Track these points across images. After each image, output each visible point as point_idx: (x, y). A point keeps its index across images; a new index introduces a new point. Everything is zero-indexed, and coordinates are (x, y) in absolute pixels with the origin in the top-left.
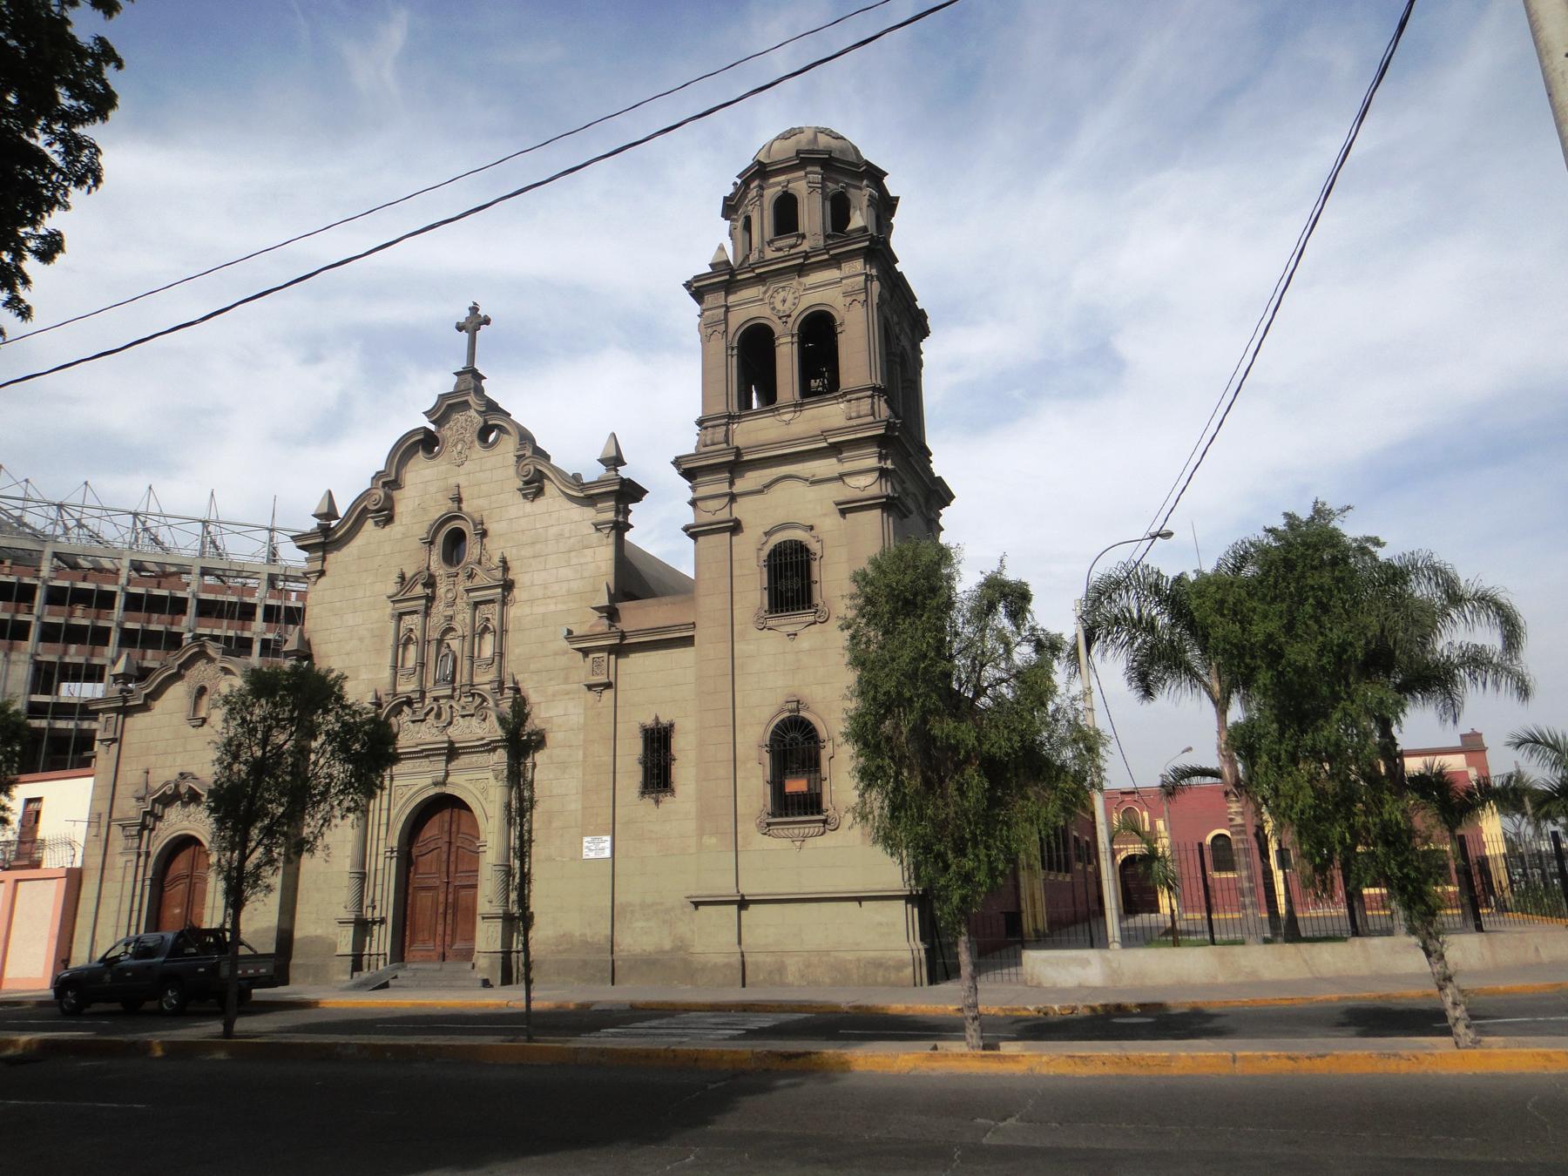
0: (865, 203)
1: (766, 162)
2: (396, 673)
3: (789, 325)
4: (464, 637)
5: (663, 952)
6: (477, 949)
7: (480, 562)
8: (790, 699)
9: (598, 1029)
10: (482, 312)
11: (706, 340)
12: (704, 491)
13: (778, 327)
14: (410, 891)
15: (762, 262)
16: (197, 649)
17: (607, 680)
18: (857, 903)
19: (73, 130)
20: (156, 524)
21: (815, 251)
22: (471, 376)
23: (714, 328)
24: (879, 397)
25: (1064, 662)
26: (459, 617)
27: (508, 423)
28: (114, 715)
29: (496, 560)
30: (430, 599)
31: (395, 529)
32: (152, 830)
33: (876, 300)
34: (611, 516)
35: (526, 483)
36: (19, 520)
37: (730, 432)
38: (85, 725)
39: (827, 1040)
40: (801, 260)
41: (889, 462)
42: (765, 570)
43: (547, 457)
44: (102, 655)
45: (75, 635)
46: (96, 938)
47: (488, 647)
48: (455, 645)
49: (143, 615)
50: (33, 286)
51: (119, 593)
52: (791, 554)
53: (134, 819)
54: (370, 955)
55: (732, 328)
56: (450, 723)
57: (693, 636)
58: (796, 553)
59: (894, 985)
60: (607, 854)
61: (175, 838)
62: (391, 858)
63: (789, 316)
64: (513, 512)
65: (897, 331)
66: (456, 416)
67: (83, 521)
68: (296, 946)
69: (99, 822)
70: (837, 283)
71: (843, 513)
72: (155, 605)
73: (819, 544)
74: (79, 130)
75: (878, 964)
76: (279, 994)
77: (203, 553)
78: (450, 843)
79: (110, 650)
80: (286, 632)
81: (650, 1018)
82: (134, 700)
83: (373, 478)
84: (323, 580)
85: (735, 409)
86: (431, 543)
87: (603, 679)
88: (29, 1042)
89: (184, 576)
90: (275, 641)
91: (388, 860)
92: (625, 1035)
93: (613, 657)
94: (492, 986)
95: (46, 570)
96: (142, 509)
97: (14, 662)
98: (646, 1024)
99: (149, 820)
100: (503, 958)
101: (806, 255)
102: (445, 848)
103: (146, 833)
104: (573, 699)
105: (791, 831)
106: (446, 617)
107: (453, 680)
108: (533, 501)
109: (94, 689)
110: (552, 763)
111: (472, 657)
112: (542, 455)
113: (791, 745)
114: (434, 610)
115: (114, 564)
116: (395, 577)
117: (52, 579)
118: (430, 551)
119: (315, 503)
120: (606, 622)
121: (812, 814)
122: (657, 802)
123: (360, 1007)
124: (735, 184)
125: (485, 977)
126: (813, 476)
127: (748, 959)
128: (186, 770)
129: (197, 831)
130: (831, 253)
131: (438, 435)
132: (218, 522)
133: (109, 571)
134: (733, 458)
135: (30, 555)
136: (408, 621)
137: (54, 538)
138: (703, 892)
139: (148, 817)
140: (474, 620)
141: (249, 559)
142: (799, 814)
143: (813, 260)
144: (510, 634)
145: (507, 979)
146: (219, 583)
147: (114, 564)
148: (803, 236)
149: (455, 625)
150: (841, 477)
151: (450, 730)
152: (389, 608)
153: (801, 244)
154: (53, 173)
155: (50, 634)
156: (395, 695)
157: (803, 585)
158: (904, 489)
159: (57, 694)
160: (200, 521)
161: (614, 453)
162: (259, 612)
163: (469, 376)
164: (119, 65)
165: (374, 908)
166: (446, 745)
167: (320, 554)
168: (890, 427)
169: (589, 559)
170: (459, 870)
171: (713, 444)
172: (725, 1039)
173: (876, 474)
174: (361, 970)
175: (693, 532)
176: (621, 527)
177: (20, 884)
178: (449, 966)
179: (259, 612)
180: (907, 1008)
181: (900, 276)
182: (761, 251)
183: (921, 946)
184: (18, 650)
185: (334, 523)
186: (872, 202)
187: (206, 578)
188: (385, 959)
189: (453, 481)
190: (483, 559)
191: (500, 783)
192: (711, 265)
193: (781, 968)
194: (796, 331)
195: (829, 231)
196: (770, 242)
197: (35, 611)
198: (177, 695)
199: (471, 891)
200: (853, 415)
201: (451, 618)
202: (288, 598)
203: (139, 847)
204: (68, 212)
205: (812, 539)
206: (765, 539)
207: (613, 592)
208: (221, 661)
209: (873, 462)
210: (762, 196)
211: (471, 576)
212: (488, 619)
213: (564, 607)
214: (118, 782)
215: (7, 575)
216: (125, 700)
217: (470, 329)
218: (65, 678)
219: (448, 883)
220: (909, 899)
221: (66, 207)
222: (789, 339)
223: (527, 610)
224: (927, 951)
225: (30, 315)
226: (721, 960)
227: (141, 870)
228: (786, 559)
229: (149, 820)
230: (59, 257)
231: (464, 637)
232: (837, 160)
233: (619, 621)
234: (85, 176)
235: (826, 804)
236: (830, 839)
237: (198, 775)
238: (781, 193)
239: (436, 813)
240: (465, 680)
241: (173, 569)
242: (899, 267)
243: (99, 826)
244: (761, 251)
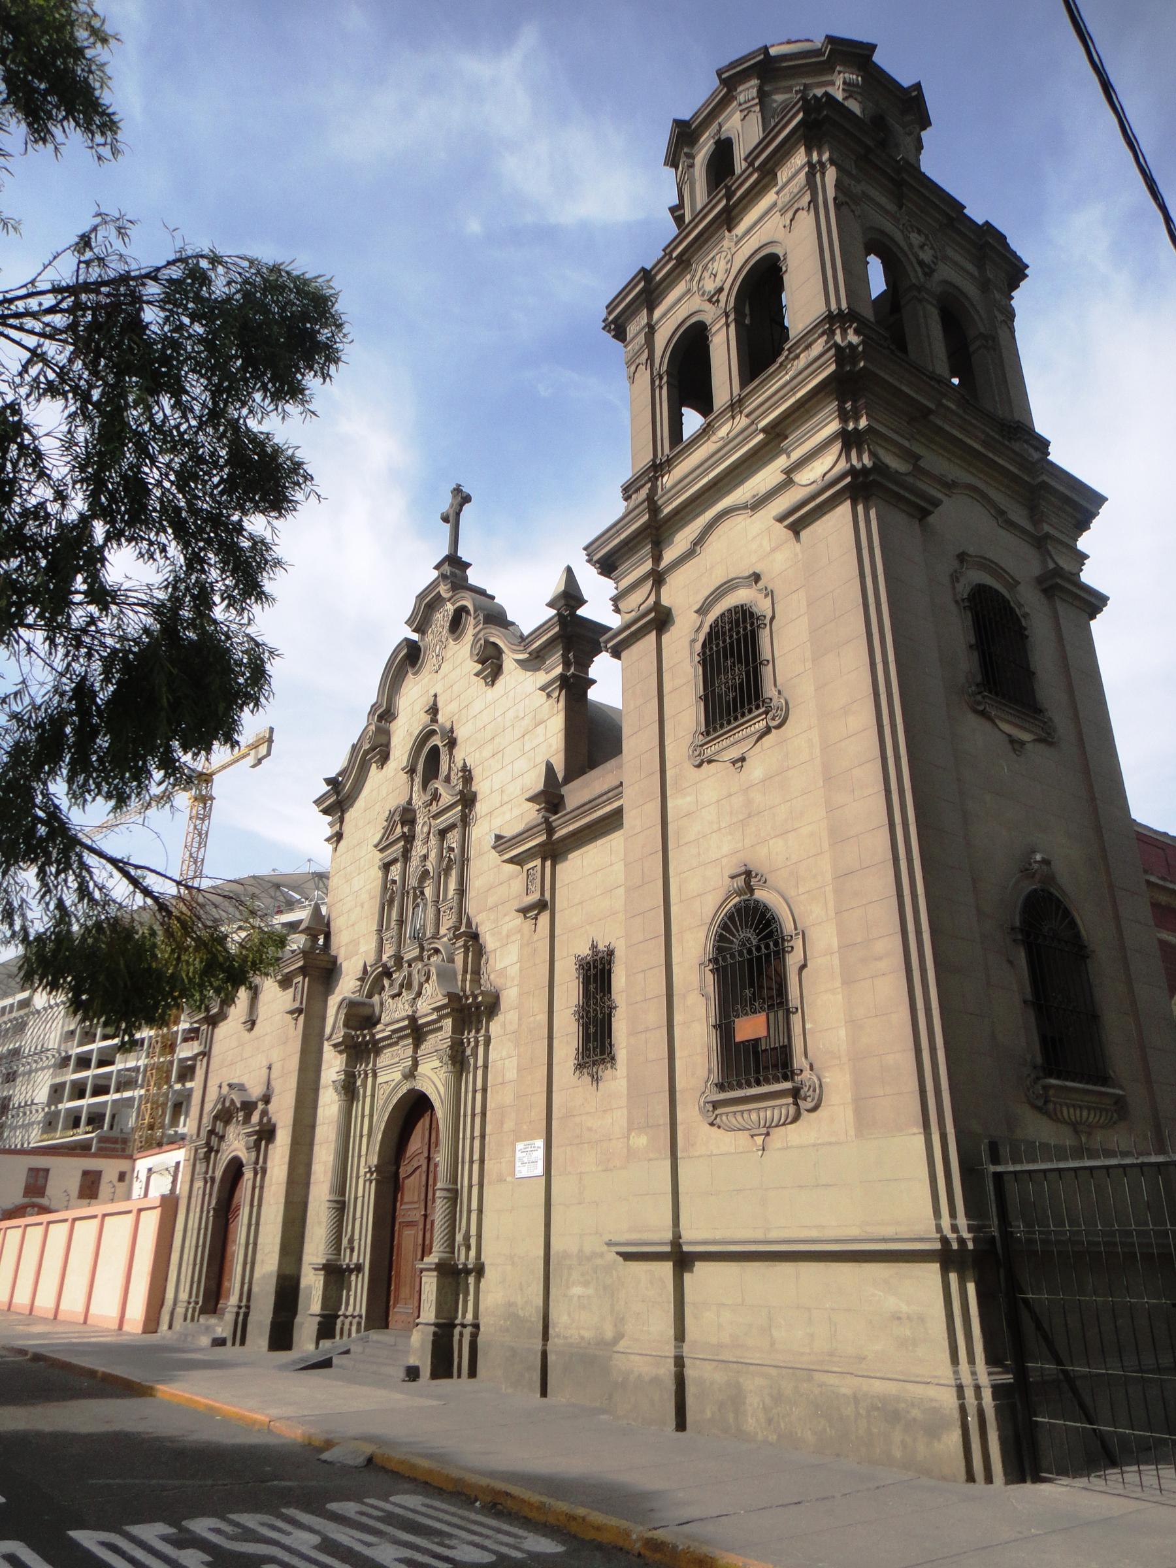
25: (843, 465)
32: (217, 1152)
52: (731, 630)
54: (346, 1317)
58: (738, 625)
64: (478, 706)
99: (214, 1141)
100: (435, 1334)
110: (505, 1035)
144: (472, 863)
166: (406, 1023)
173: (837, 447)
174: (333, 1337)
235: (799, 1061)
238: (714, 147)
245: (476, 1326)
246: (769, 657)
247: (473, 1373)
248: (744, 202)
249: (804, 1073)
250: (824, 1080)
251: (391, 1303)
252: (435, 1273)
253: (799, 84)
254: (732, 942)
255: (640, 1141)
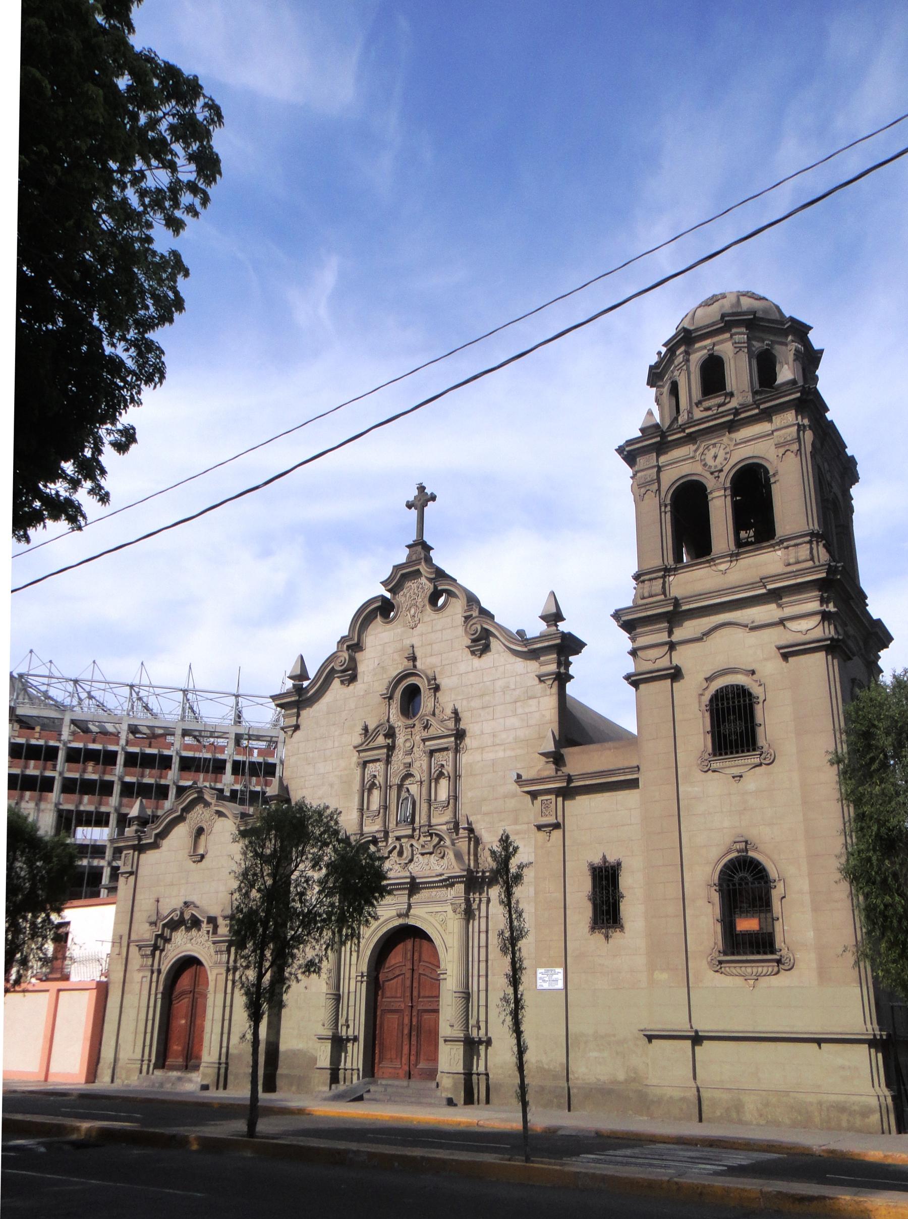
0: (791, 357)
1: (692, 328)
2: (362, 815)
3: (722, 479)
4: (421, 782)
5: (615, 1082)
6: (440, 1069)
7: (434, 714)
8: (737, 840)
9: (578, 1154)
10: (428, 491)
11: (639, 499)
12: (642, 641)
13: (710, 483)
14: (379, 1013)
15: (691, 422)
16: (196, 795)
17: (555, 821)
18: (815, 1045)
19: (146, 336)
20: (146, 694)
21: (745, 407)
22: (421, 548)
23: (648, 488)
24: (817, 542)
26: (417, 764)
27: (456, 587)
28: (131, 852)
29: (449, 712)
30: (391, 748)
31: (358, 687)
33: (809, 448)
34: (553, 667)
35: (473, 641)
36: (46, 694)
37: (667, 585)
38: (95, 863)
39: (818, 1183)
40: (731, 417)
41: (831, 605)
42: (707, 715)
43: (492, 617)
44: (107, 804)
45: (87, 787)
46: (120, 1042)
47: (443, 791)
48: (414, 789)
49: (138, 770)
50: (108, 476)
51: (119, 752)
52: (733, 698)
53: (147, 941)
55: (665, 486)
56: (411, 861)
57: (638, 779)
59: (859, 1131)
60: (560, 985)
61: (185, 956)
62: (362, 982)
63: (721, 471)
64: (463, 667)
65: (829, 479)
66: (408, 584)
67: (92, 693)
68: (282, 1057)
69: (120, 943)
70: (768, 435)
71: (785, 657)
72: (147, 761)
73: (761, 689)
74: (150, 335)
75: (842, 1108)
76: (271, 1100)
77: (184, 717)
78: (413, 970)
79: (114, 800)
80: (250, 782)
81: (628, 1146)
82: (146, 839)
83: (339, 643)
84: (298, 733)
85: (670, 562)
86: (390, 698)
87: (551, 820)
88: (89, 1130)
89: (168, 737)
90: (241, 791)
91: (359, 984)
92: (605, 1162)
93: (560, 799)
94: (456, 1105)
95: (65, 735)
96: (136, 682)
97: (43, 811)
98: (618, 1152)
99: (160, 942)
101: (736, 412)
102: (408, 975)
103: (157, 953)
104: (523, 838)
105: (743, 969)
106: (405, 764)
107: (413, 821)
108: (480, 657)
109: (101, 833)
111: (429, 801)
112: (485, 614)
113: (740, 884)
114: (394, 759)
115: (115, 728)
116: (359, 729)
117: (70, 741)
118: (389, 706)
119: (290, 666)
120: (553, 767)
121: (765, 953)
122: (607, 937)
123: (345, 1115)
124: (659, 353)
125: (450, 1096)
126: (753, 622)
127: (705, 1094)
128: (187, 899)
129: (199, 953)
130: (762, 407)
131: (394, 602)
132: (195, 691)
133: (111, 734)
134: (671, 608)
135: (54, 722)
136: (372, 768)
137: (72, 708)
138: (656, 1026)
139: (159, 939)
140: (431, 765)
141: (219, 721)
142: (753, 954)
143: (743, 416)
144: (462, 779)
145: (469, 1099)
146: (196, 743)
147: (115, 728)
148: (731, 395)
149: (413, 771)
150: (782, 622)
151: (411, 867)
152: (355, 758)
153: (729, 402)
154: (128, 376)
155: (69, 786)
156: (362, 834)
157: (746, 728)
158: (846, 633)
159: (74, 837)
160: (181, 690)
161: (554, 610)
162: (229, 767)
163: (419, 548)
164: (187, 274)
165: (348, 1027)
166: (408, 880)
167: (295, 710)
168: (831, 570)
169: (534, 709)
170: (422, 995)
171: (651, 596)
172: (711, 1174)
173: (818, 618)
175: (635, 681)
176: (562, 678)
177: (61, 993)
178: (415, 1084)
179: (229, 767)
180: (885, 1156)
181: (831, 424)
182: (690, 412)
183: (887, 1093)
184: (46, 800)
185: (306, 684)
186: (798, 355)
187: (186, 738)
188: (358, 1074)
189: (407, 643)
190: (437, 711)
191: (459, 916)
192: (642, 430)
193: (739, 1107)
194: (728, 485)
195: (757, 386)
196: (698, 404)
197: (58, 768)
198: (181, 834)
199: (432, 1016)
200: (792, 561)
201: (410, 765)
202: (251, 754)
203: (152, 965)
204: (141, 408)
205: (754, 683)
206: (705, 685)
207: (557, 738)
208: (216, 805)
209: (815, 606)
210: (688, 361)
211: (426, 727)
212: (442, 766)
213: (512, 754)
214: (135, 909)
215: (37, 739)
216: (140, 839)
217: (419, 506)
218: (80, 823)
219: (412, 1007)
220: (873, 1043)
221: (139, 403)
222: (722, 492)
223: (477, 757)
224: (894, 1098)
225: (108, 500)
226: (677, 1094)
227: (154, 985)
228: (728, 703)
229: (160, 942)
230: (133, 447)
231: (421, 782)
232: (762, 319)
233: (565, 765)
234: (153, 374)
235: (779, 943)
236: (783, 980)
237: (198, 903)
238: (707, 356)
239: (399, 943)
240: (424, 821)
241: (160, 731)
242: (829, 416)
243: (121, 947)
244: (690, 412)
245: (487, 1075)
246: (762, 723)
247: (488, 1101)
248: (744, 421)
249: (782, 952)
250: (796, 956)
251: (376, 1061)
252: (462, 1043)
253: (768, 340)
254: (733, 877)
255: (662, 976)
